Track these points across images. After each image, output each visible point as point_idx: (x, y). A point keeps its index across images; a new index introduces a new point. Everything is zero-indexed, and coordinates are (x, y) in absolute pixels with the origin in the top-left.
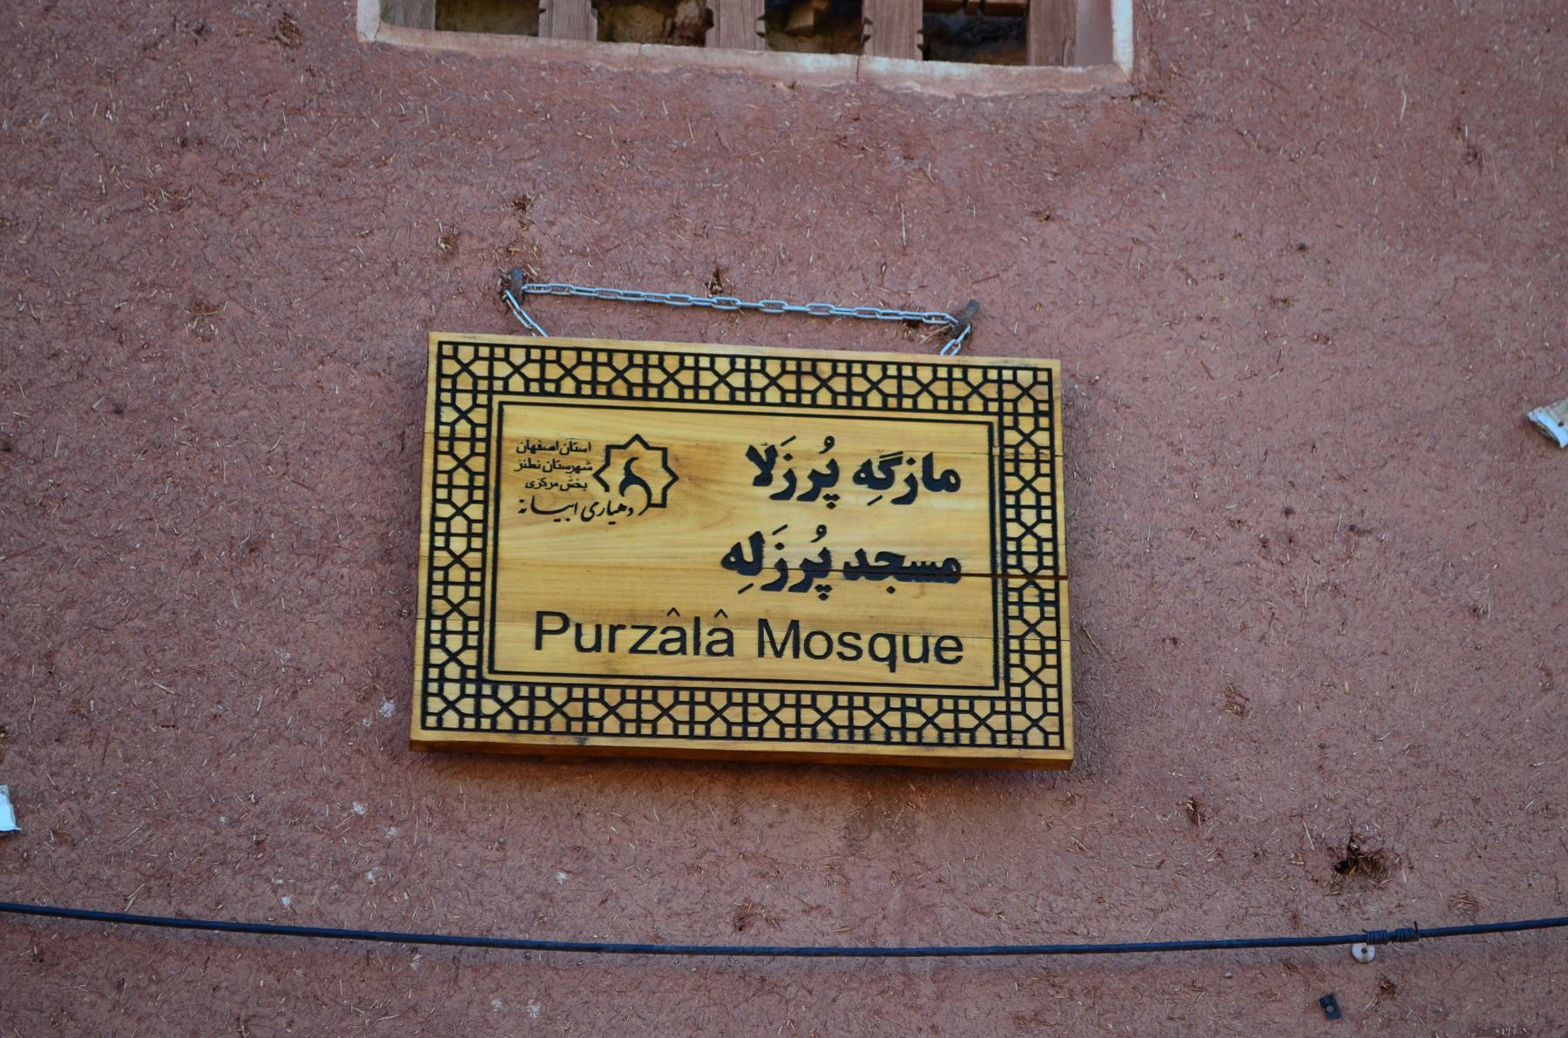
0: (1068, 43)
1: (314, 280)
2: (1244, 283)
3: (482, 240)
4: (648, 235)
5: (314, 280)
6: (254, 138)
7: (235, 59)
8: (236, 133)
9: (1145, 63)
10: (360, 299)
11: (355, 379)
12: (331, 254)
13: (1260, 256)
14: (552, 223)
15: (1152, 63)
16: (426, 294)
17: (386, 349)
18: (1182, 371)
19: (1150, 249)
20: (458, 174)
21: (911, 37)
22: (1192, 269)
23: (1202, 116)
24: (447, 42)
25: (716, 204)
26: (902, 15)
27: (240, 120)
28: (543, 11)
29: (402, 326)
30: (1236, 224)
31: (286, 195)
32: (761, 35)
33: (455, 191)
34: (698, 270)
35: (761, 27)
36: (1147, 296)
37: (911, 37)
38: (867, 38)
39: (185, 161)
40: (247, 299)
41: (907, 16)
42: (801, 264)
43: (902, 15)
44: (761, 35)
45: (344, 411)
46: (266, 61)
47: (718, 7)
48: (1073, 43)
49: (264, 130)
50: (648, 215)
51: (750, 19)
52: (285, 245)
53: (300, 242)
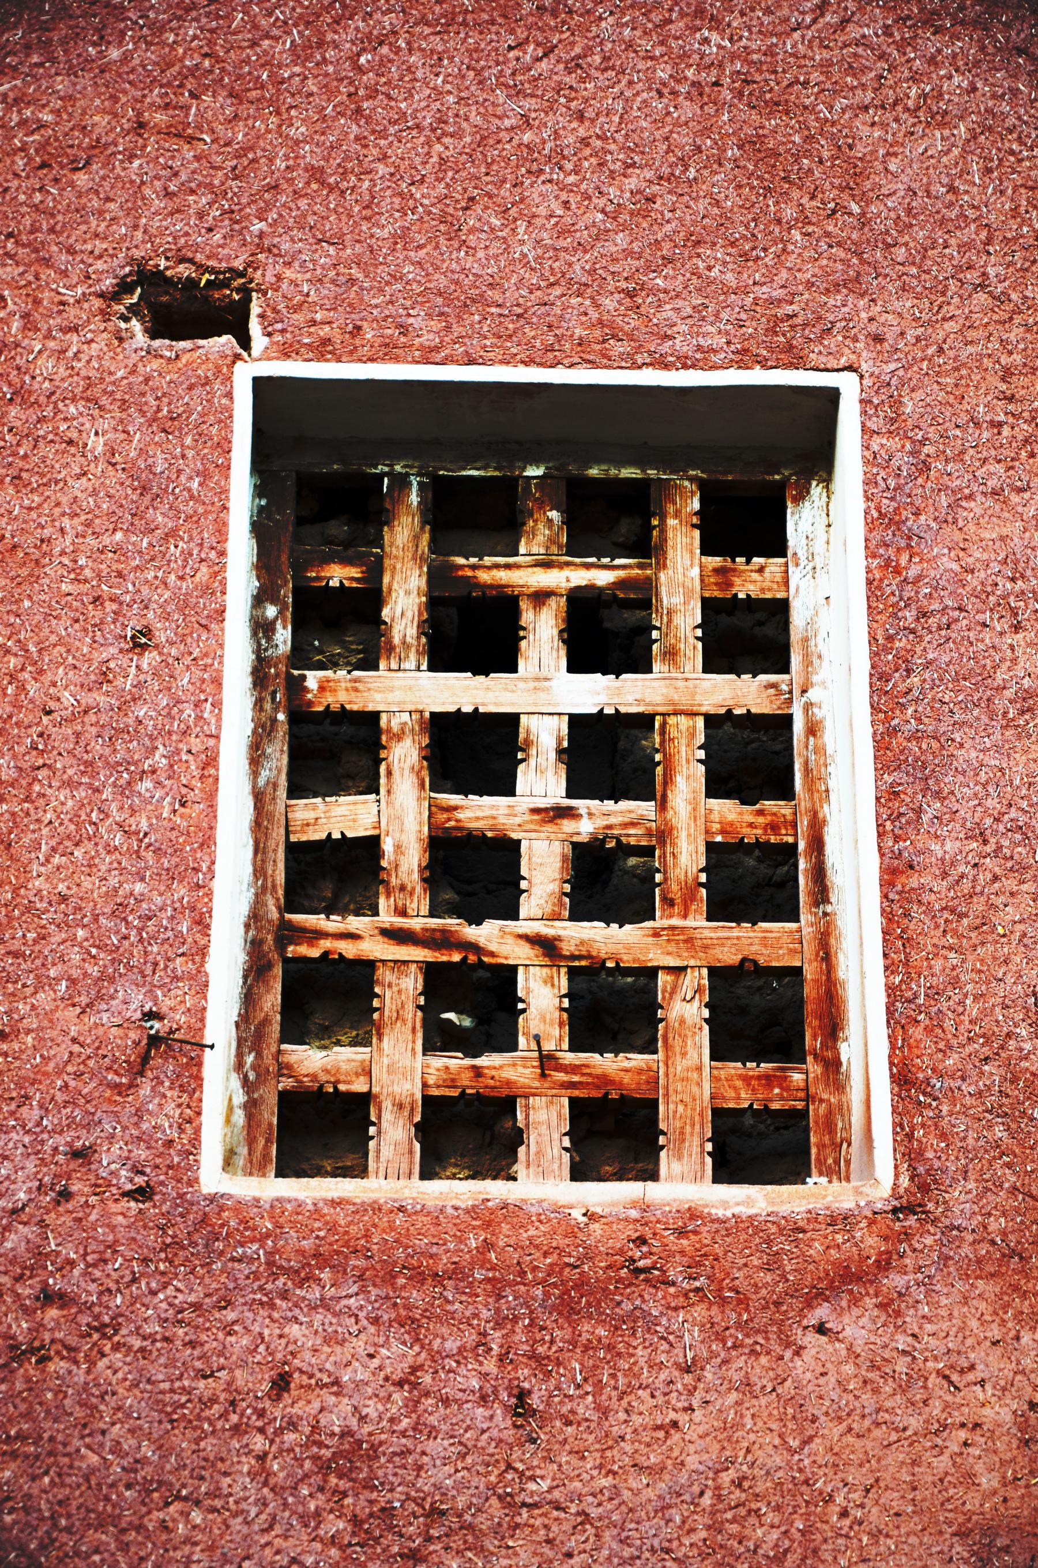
0: (845, 1145)
1: (160, 1422)
2: (1004, 1389)
3: (311, 1376)
4: (458, 1362)
5: (160, 1422)
6: (109, 1290)
7: (93, 1217)
8: (93, 1287)
9: (905, 1181)
10: (202, 1439)
11: (197, 1517)
12: (176, 1397)
13: (1018, 1363)
14: (371, 1356)
15: (912, 1179)
16: (261, 1430)
17: (225, 1485)
18: (949, 1478)
19: (914, 1358)
20: (290, 1314)
21: (702, 1146)
22: (955, 1377)
23: (958, 1228)
24: (274, 1188)
25: (517, 1330)
26: (693, 1125)
27: (97, 1274)
28: (372, 1138)
29: (239, 1462)
30: (995, 1332)
31: (137, 1343)
32: (565, 1149)
33: (286, 1330)
34: (504, 1396)
35: (567, 1142)
36: (913, 1404)
37: (702, 1146)
38: (663, 1147)
39: (47, 1317)
40: (102, 1445)
41: (697, 1127)
42: (594, 1385)
43: (693, 1125)
44: (565, 1149)
45: (187, 1549)
46: (120, 1218)
47: (527, 1125)
48: (849, 1145)
49: (117, 1282)
50: (458, 1344)
51: (556, 1136)
52: (136, 1392)
53: (149, 1387)
